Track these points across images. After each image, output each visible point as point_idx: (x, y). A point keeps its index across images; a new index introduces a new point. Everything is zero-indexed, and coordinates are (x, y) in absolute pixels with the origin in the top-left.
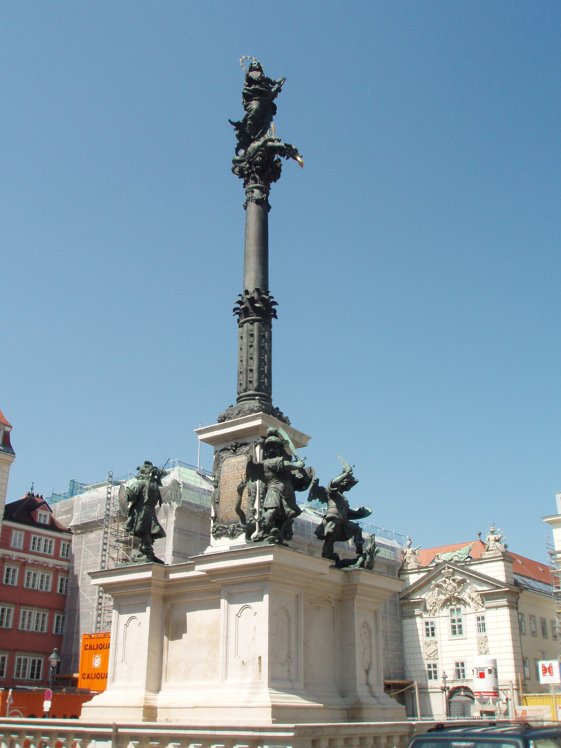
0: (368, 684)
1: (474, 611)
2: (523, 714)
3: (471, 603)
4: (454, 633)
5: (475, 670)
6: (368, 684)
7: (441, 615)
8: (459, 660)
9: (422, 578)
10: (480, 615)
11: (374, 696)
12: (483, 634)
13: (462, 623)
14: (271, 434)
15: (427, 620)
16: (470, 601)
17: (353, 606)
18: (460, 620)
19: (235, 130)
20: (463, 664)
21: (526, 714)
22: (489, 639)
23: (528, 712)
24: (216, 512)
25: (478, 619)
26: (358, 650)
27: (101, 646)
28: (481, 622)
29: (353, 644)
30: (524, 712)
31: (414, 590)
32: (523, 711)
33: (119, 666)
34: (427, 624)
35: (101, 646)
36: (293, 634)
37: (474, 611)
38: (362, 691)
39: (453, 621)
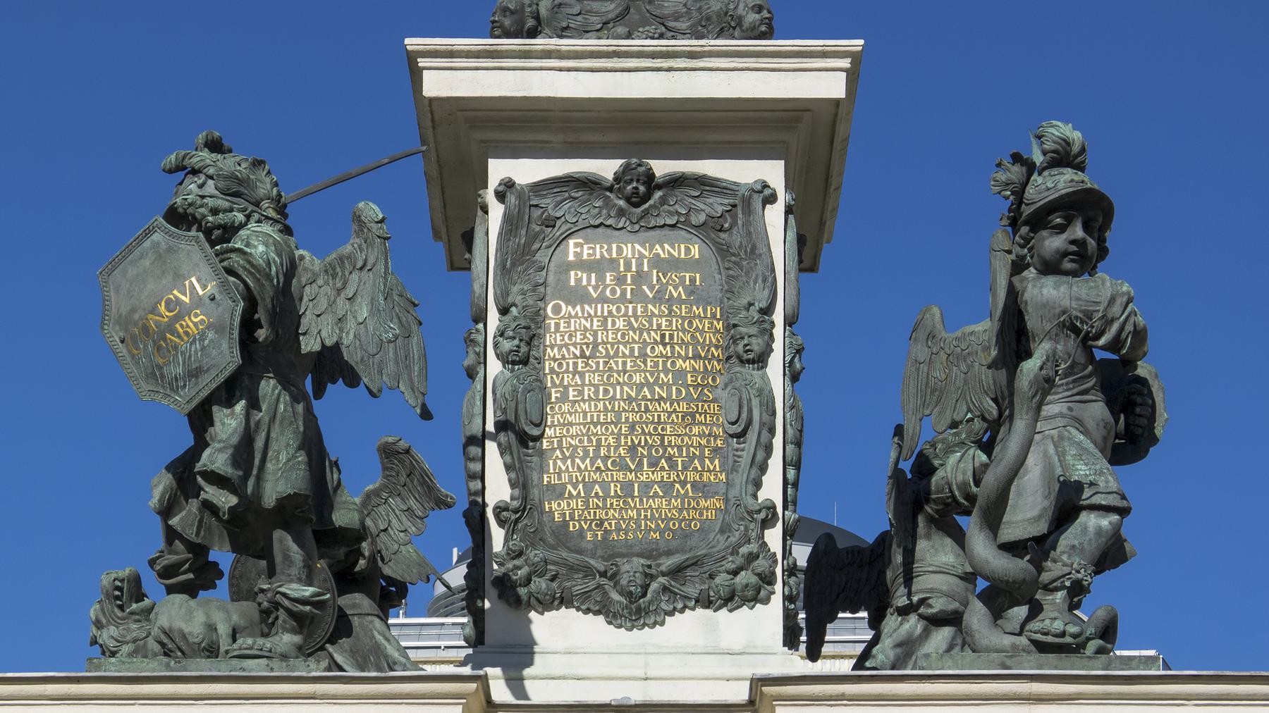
14: (609, 451)
24: (520, 481)
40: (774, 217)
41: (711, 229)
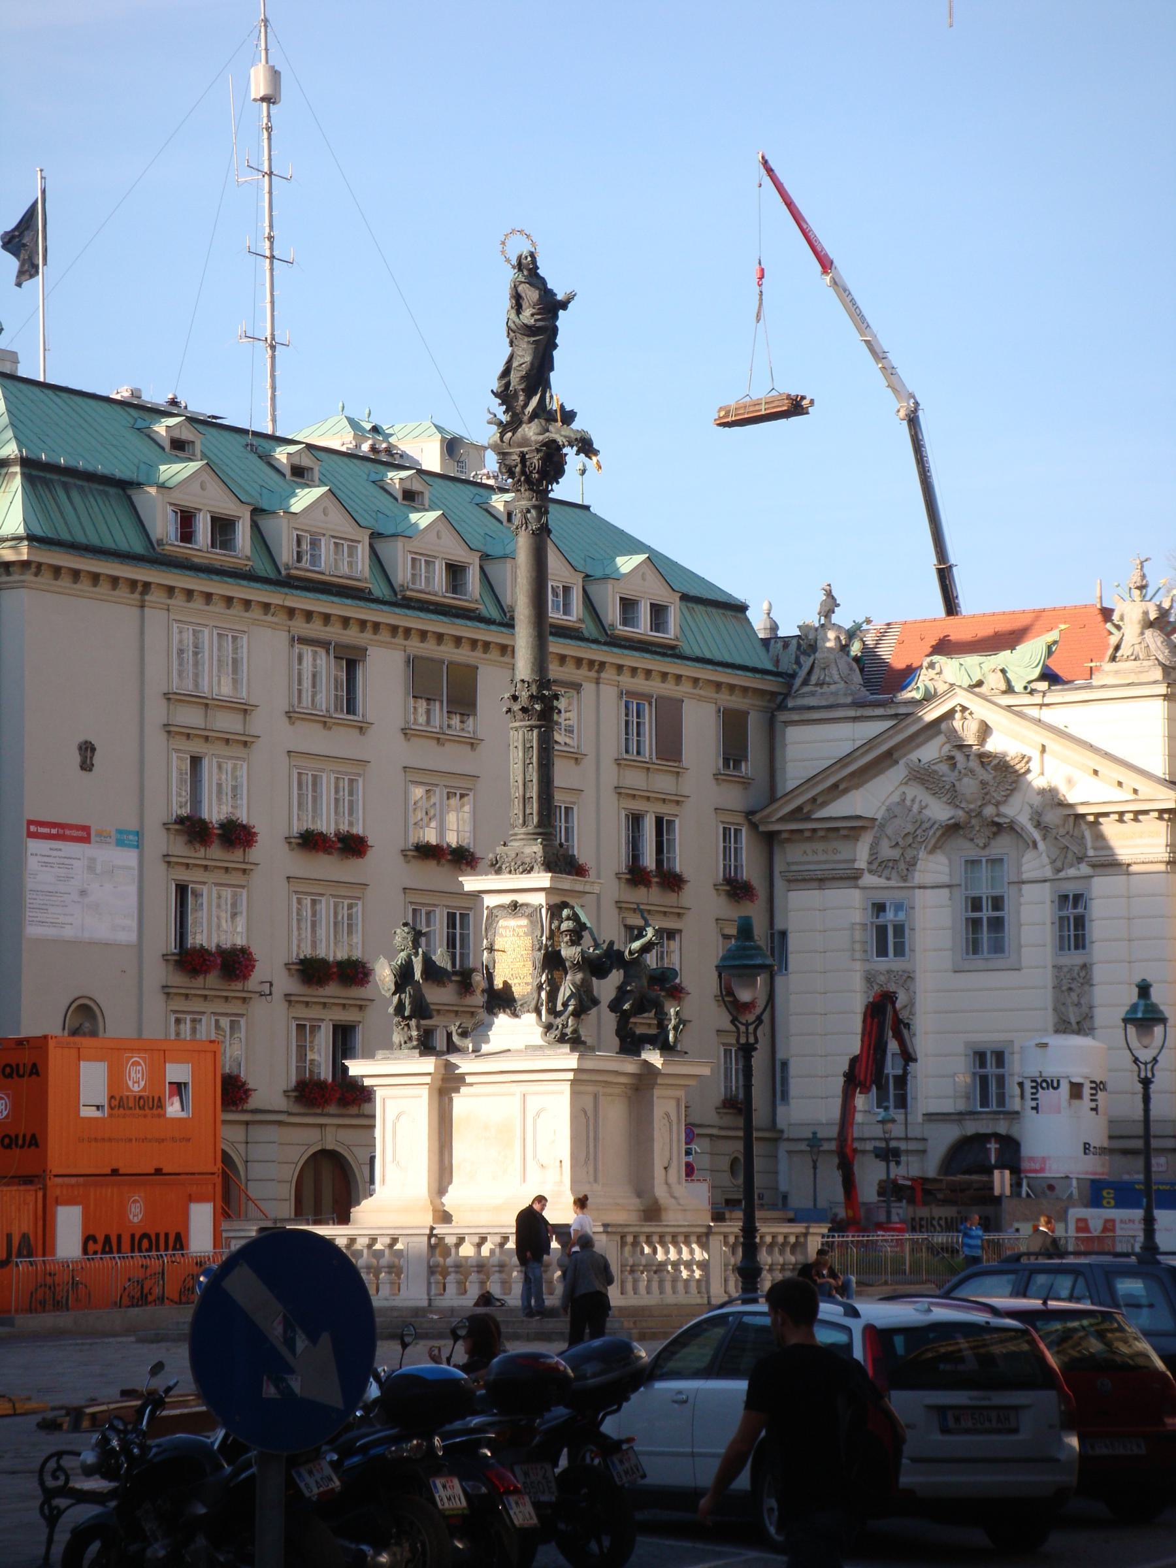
0: (667, 1183)
1: (1048, 873)
2: (1105, 1229)
3: (1041, 845)
4: (974, 947)
5: (1028, 1085)
6: (667, 1183)
7: (929, 879)
8: (989, 1038)
9: (871, 743)
10: (1071, 888)
11: (675, 1198)
12: (1074, 959)
13: (1008, 913)
15: (880, 897)
16: (1037, 835)
17: (652, 1096)
18: (997, 903)
19: (500, 405)
20: (1000, 1057)
21: (1114, 1230)
22: (1098, 973)
23: (1118, 1226)
25: (1064, 898)
26: (657, 1146)
27: (8, 1070)
28: (1070, 912)
29: (652, 1140)
30: (1109, 1225)
31: (835, 786)
32: (1107, 1221)
33: (389, 1167)
34: (880, 908)
35: (8, 1070)
36: (591, 1134)
37: (1048, 873)
38: (660, 1192)
39: (976, 904)
40: (544, 911)
41: (530, 916)
